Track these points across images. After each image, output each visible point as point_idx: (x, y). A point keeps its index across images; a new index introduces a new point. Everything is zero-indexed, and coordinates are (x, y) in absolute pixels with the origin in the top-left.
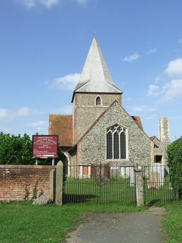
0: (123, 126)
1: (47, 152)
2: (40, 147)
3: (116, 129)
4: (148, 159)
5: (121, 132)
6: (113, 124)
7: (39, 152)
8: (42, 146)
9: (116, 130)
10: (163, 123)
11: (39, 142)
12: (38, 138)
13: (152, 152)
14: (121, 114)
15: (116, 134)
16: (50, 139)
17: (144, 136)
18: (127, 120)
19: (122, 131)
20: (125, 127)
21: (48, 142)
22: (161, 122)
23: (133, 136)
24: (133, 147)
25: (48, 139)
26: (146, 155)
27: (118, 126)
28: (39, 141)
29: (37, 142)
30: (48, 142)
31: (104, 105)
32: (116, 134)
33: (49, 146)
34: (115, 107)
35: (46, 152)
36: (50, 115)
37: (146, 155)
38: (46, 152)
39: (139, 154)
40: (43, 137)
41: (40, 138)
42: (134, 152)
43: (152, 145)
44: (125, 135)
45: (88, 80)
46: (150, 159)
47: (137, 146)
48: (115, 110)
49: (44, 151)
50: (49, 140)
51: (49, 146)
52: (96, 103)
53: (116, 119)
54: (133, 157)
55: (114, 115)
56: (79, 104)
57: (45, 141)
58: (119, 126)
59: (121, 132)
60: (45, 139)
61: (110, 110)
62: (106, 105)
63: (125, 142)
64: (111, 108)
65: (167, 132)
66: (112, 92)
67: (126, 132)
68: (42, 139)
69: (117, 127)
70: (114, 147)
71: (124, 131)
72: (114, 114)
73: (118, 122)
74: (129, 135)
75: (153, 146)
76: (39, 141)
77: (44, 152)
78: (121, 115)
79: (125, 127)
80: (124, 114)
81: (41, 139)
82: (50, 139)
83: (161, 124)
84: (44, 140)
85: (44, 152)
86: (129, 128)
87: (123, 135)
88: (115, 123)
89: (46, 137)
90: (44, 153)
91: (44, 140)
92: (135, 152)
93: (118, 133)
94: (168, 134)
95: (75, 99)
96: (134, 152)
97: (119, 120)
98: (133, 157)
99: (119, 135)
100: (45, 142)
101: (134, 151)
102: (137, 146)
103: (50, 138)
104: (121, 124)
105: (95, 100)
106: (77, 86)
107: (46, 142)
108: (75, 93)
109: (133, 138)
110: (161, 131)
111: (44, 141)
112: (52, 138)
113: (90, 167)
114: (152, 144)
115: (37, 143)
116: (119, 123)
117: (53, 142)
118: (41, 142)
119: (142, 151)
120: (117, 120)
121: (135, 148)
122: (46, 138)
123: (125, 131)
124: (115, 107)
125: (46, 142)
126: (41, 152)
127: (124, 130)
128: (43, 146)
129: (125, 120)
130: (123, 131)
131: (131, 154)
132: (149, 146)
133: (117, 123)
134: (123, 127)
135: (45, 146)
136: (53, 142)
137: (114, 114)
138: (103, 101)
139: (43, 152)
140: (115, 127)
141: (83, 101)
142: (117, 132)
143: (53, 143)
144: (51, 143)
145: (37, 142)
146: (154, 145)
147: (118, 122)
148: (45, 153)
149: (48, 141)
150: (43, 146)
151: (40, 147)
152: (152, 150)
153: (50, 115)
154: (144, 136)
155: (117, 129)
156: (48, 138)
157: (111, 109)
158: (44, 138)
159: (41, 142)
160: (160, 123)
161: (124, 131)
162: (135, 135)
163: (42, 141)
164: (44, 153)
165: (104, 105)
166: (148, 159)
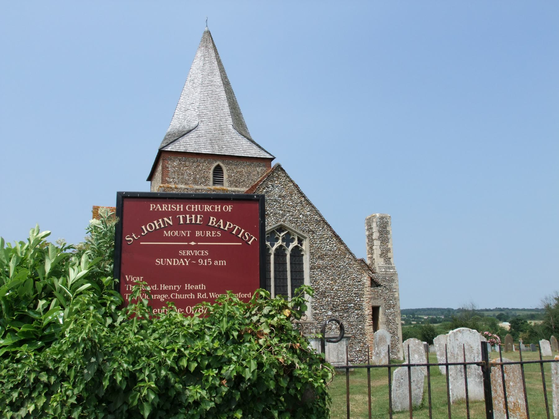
0: (296, 230)
1: (203, 287)
2: (159, 262)
3: (281, 238)
4: (356, 316)
5: (292, 246)
6: (274, 226)
7: (155, 287)
8: (173, 252)
9: (280, 242)
10: (378, 228)
11: (157, 235)
12: (152, 207)
13: (366, 298)
14: (291, 200)
15: (280, 252)
16: (218, 216)
17: (347, 256)
18: (307, 216)
19: (295, 243)
20: (303, 234)
21: (208, 234)
22: (374, 225)
23: (321, 258)
24: (322, 284)
25: (206, 216)
26: (352, 305)
27: (283, 231)
28: (156, 225)
29: (146, 229)
30: (208, 234)
31: (231, 185)
32: (280, 252)
33: (215, 253)
34: (276, 182)
35: (197, 287)
36: (119, 194)
37: (352, 305)
38: (197, 287)
39: (335, 303)
40: (179, 207)
41: (165, 207)
42: (324, 299)
43: (366, 281)
44: (303, 254)
45: (193, 125)
46: (362, 316)
47: (330, 282)
48: (277, 189)
49: (188, 287)
50: (212, 220)
51: (215, 253)
52: (211, 179)
53: (281, 212)
54: (323, 310)
55: (275, 203)
56: (171, 180)
57: (193, 227)
58: (286, 230)
59: (292, 246)
60: (191, 214)
61: (264, 189)
62: (236, 187)
63: (301, 272)
64: (267, 184)
65: (388, 250)
66: (250, 156)
67: (304, 247)
68: (174, 214)
69: (282, 234)
70: (275, 286)
71: (299, 245)
72: (276, 201)
73: (284, 221)
74: (312, 254)
75: (368, 283)
76: (156, 225)
77: (188, 292)
78: (291, 203)
79: (301, 233)
80: (299, 201)
81: (166, 214)
82: (218, 216)
83: (374, 230)
84: (185, 219)
85: (188, 292)
86: (311, 238)
87: (297, 253)
88: (279, 224)
89: (196, 207)
90: (186, 296)
91: (185, 219)
92: (326, 297)
93: (284, 250)
94: (389, 255)
95: (160, 168)
96: (324, 299)
97: (288, 215)
98: (323, 310)
99: (286, 255)
100: (193, 234)
101: (323, 294)
102: (330, 282)
103: (218, 208)
104: (292, 226)
105: (211, 171)
106: (165, 139)
107: (198, 234)
108: (162, 153)
109: (321, 262)
110: (374, 247)
111: (185, 227)
112: (229, 208)
113: (426, 367)
114: (365, 278)
115: (144, 238)
116: (287, 224)
117: (239, 231)
118: (170, 233)
119: (342, 295)
120: (283, 216)
121: (326, 288)
122: (198, 213)
123: (301, 245)
124: (276, 182)
125: (198, 234)
126: (168, 292)
127: (300, 241)
128: (179, 257)
129: (301, 216)
130: (296, 244)
131: (317, 304)
132: (359, 283)
133: (283, 223)
134: (295, 232)
135: (196, 258)
136: (239, 231)
137: (276, 201)
138: (230, 176)
139: (182, 291)
140: (278, 233)
141: (182, 174)
142: (281, 246)
143: (235, 238)
144: (228, 235)
145: (146, 229)
146: (369, 279)
147: (284, 221)
148: (192, 296)
149: (205, 226)
150: (182, 253)
151: (159, 262)
152: (366, 293)
153: (119, 194)
154: (347, 256)
155: (283, 240)
156: (208, 208)
157: (268, 188)
158: (185, 212)
159: (170, 233)
160: (371, 228)
161: (298, 244)
162: (326, 255)
163: (177, 226)
164: (186, 296)
165: (231, 185)
166: (356, 316)
